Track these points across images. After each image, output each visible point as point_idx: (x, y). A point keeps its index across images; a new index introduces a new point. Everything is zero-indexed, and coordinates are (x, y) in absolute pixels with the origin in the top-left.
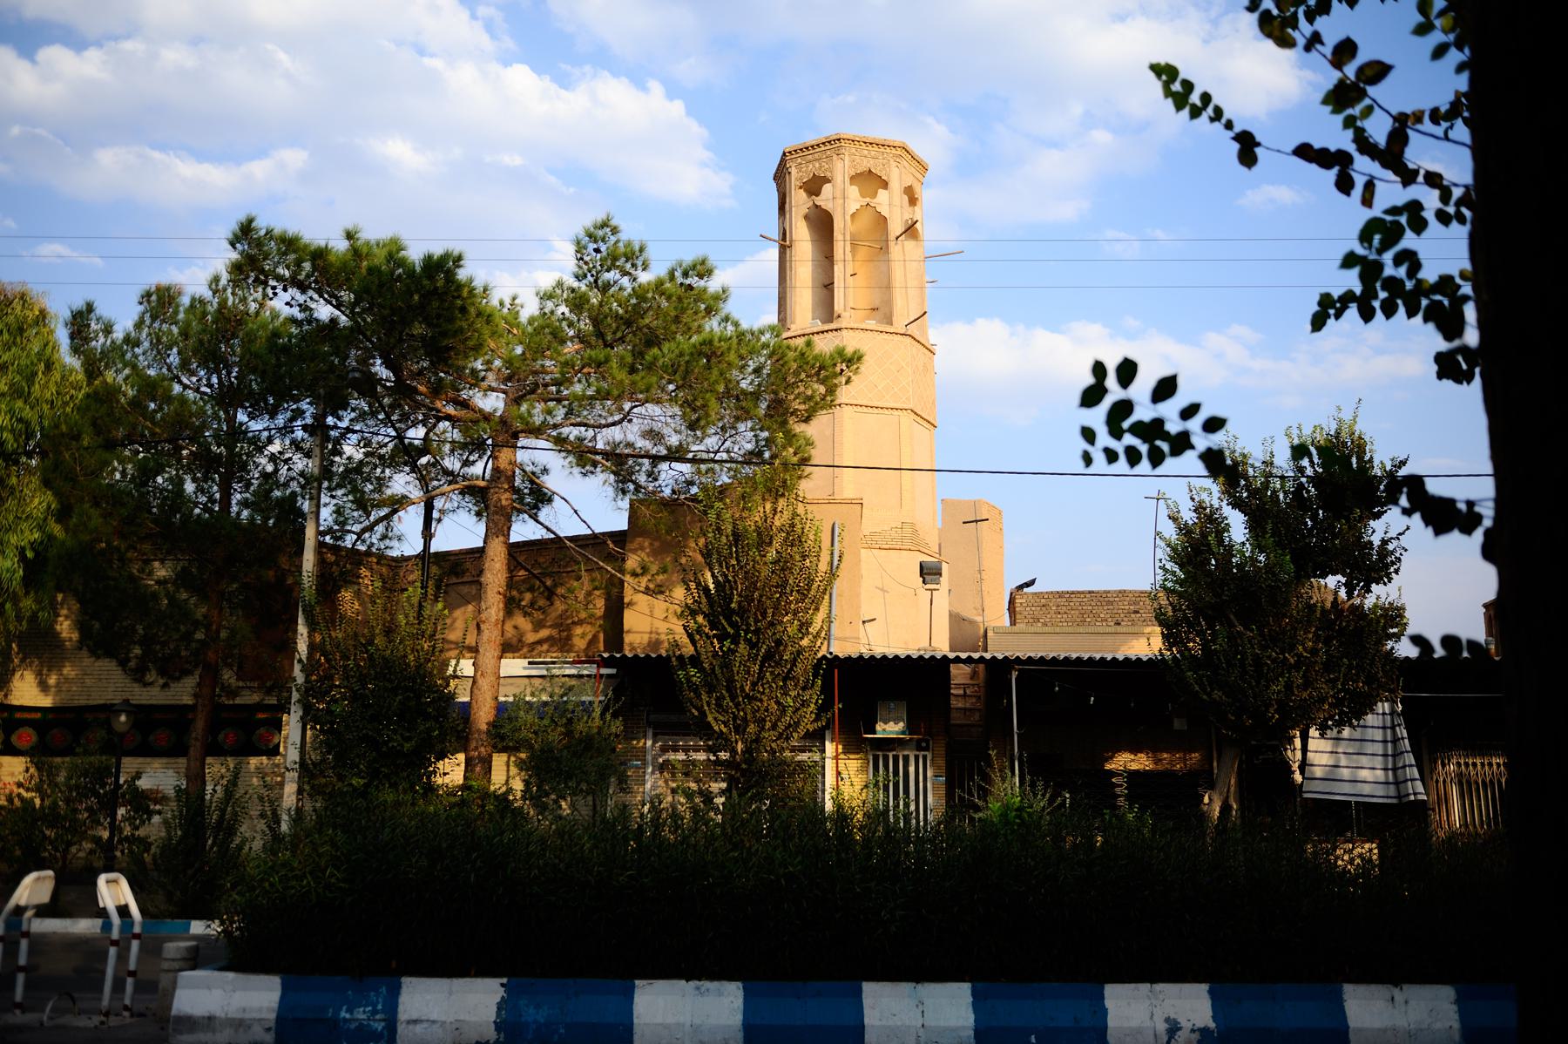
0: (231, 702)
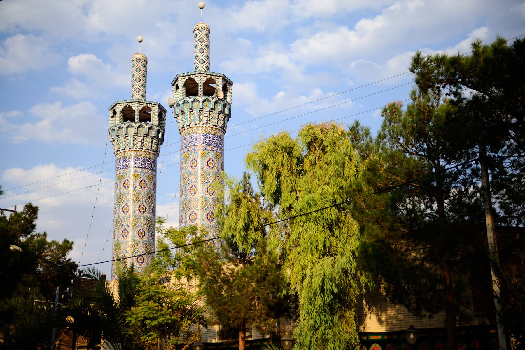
0: (468, 325)
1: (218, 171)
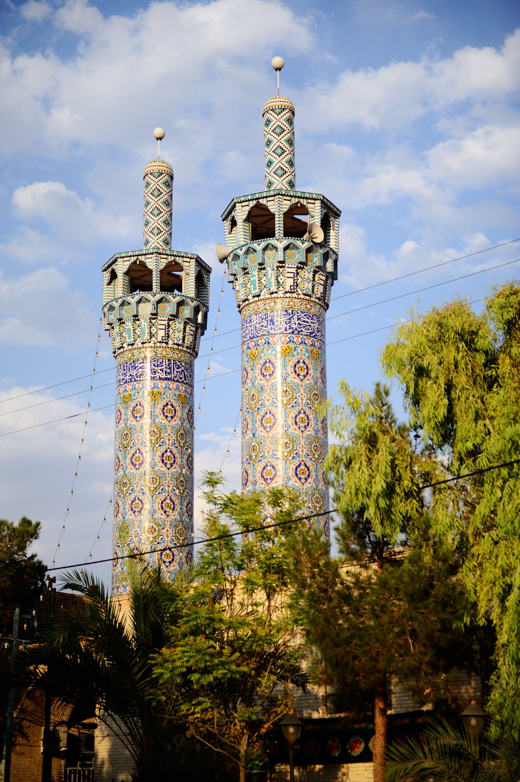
1: (316, 383)
